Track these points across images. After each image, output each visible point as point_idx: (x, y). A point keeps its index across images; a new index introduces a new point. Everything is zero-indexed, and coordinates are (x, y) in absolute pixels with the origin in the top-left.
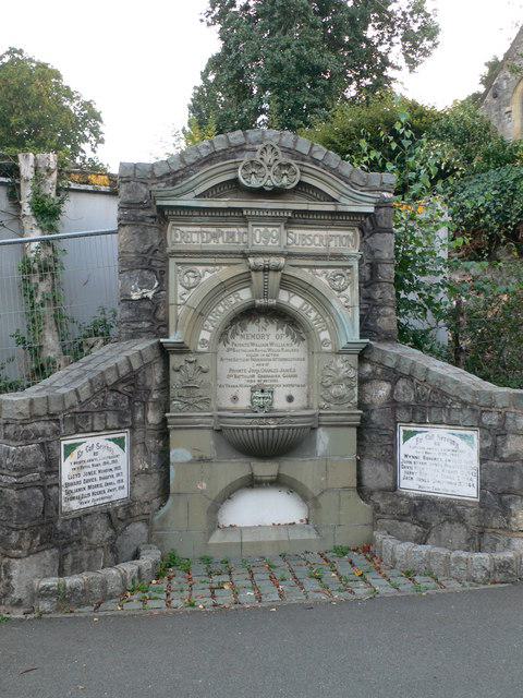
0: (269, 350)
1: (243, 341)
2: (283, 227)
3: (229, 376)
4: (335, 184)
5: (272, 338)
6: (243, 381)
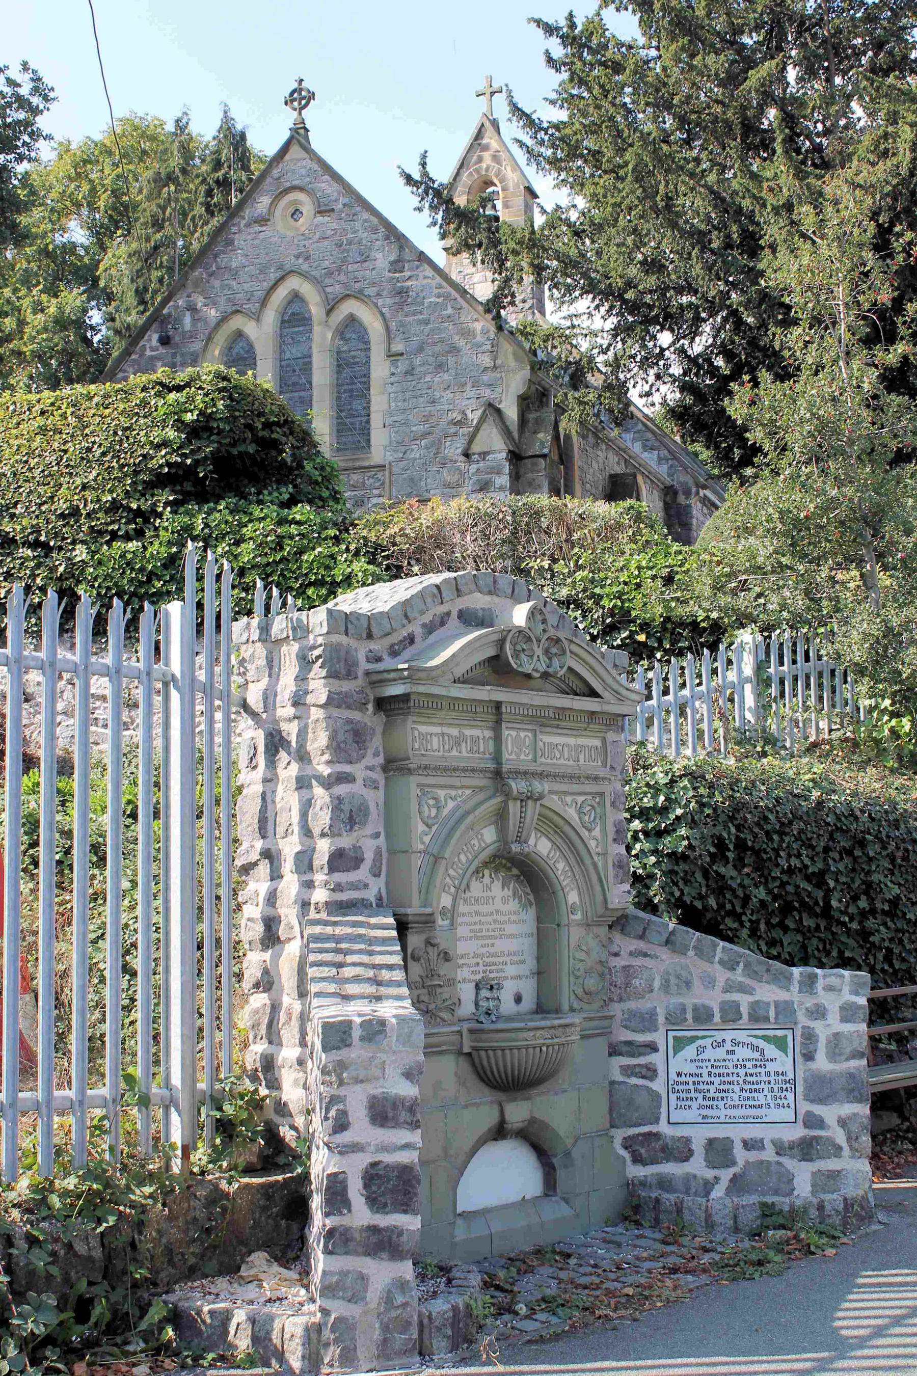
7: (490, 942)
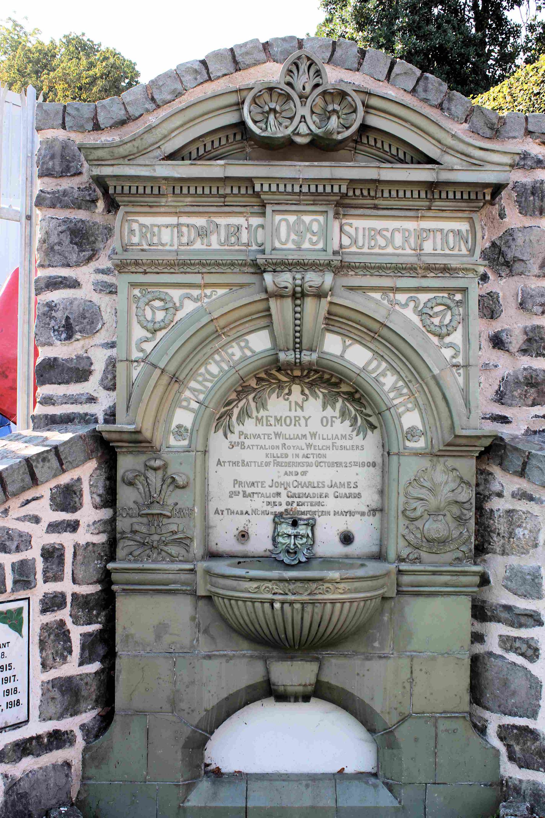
0: (309, 446)
1: (261, 429)
2: (331, 214)
3: (232, 494)
6: (258, 503)
7: (300, 469)
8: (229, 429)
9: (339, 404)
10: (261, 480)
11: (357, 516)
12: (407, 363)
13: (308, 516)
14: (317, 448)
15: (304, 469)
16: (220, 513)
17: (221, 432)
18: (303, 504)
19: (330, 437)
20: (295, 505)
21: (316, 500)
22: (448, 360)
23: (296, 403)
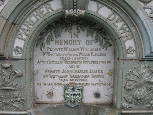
0: (80, 54)
1: (58, 46)
3: (45, 76)
4: (118, 12)
5: (83, 44)
6: (57, 80)
7: (76, 65)
8: (43, 46)
9: (94, 35)
10: (58, 70)
11: (103, 85)
12: (129, 16)
13: (80, 86)
14: (84, 55)
15: (78, 64)
16: (40, 85)
17: (39, 47)
18: (78, 80)
19: (90, 50)
20: (74, 81)
21: (84, 78)
22: (148, 14)
23: (75, 34)
